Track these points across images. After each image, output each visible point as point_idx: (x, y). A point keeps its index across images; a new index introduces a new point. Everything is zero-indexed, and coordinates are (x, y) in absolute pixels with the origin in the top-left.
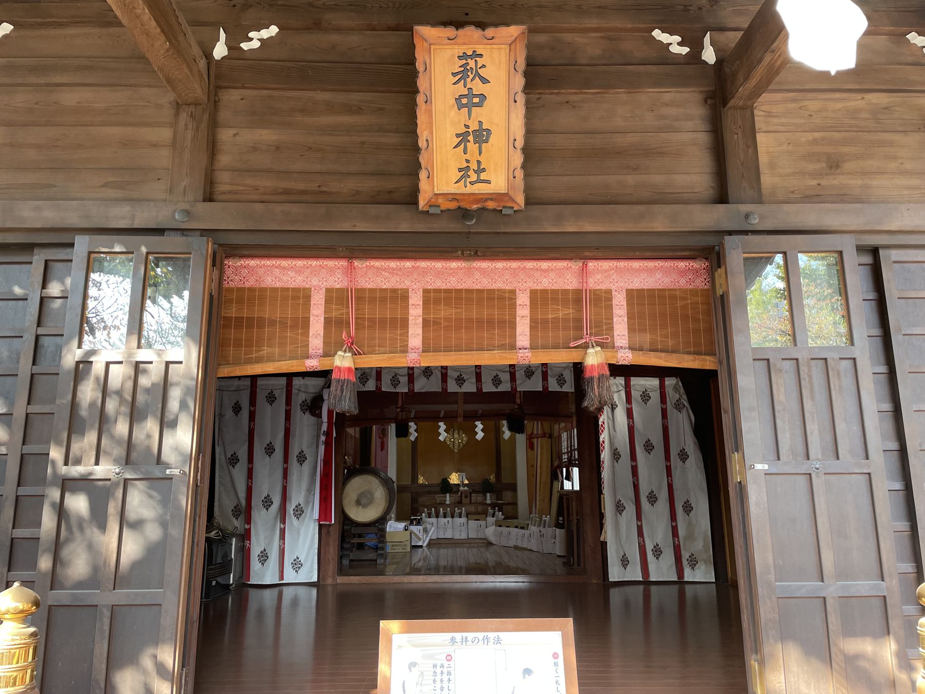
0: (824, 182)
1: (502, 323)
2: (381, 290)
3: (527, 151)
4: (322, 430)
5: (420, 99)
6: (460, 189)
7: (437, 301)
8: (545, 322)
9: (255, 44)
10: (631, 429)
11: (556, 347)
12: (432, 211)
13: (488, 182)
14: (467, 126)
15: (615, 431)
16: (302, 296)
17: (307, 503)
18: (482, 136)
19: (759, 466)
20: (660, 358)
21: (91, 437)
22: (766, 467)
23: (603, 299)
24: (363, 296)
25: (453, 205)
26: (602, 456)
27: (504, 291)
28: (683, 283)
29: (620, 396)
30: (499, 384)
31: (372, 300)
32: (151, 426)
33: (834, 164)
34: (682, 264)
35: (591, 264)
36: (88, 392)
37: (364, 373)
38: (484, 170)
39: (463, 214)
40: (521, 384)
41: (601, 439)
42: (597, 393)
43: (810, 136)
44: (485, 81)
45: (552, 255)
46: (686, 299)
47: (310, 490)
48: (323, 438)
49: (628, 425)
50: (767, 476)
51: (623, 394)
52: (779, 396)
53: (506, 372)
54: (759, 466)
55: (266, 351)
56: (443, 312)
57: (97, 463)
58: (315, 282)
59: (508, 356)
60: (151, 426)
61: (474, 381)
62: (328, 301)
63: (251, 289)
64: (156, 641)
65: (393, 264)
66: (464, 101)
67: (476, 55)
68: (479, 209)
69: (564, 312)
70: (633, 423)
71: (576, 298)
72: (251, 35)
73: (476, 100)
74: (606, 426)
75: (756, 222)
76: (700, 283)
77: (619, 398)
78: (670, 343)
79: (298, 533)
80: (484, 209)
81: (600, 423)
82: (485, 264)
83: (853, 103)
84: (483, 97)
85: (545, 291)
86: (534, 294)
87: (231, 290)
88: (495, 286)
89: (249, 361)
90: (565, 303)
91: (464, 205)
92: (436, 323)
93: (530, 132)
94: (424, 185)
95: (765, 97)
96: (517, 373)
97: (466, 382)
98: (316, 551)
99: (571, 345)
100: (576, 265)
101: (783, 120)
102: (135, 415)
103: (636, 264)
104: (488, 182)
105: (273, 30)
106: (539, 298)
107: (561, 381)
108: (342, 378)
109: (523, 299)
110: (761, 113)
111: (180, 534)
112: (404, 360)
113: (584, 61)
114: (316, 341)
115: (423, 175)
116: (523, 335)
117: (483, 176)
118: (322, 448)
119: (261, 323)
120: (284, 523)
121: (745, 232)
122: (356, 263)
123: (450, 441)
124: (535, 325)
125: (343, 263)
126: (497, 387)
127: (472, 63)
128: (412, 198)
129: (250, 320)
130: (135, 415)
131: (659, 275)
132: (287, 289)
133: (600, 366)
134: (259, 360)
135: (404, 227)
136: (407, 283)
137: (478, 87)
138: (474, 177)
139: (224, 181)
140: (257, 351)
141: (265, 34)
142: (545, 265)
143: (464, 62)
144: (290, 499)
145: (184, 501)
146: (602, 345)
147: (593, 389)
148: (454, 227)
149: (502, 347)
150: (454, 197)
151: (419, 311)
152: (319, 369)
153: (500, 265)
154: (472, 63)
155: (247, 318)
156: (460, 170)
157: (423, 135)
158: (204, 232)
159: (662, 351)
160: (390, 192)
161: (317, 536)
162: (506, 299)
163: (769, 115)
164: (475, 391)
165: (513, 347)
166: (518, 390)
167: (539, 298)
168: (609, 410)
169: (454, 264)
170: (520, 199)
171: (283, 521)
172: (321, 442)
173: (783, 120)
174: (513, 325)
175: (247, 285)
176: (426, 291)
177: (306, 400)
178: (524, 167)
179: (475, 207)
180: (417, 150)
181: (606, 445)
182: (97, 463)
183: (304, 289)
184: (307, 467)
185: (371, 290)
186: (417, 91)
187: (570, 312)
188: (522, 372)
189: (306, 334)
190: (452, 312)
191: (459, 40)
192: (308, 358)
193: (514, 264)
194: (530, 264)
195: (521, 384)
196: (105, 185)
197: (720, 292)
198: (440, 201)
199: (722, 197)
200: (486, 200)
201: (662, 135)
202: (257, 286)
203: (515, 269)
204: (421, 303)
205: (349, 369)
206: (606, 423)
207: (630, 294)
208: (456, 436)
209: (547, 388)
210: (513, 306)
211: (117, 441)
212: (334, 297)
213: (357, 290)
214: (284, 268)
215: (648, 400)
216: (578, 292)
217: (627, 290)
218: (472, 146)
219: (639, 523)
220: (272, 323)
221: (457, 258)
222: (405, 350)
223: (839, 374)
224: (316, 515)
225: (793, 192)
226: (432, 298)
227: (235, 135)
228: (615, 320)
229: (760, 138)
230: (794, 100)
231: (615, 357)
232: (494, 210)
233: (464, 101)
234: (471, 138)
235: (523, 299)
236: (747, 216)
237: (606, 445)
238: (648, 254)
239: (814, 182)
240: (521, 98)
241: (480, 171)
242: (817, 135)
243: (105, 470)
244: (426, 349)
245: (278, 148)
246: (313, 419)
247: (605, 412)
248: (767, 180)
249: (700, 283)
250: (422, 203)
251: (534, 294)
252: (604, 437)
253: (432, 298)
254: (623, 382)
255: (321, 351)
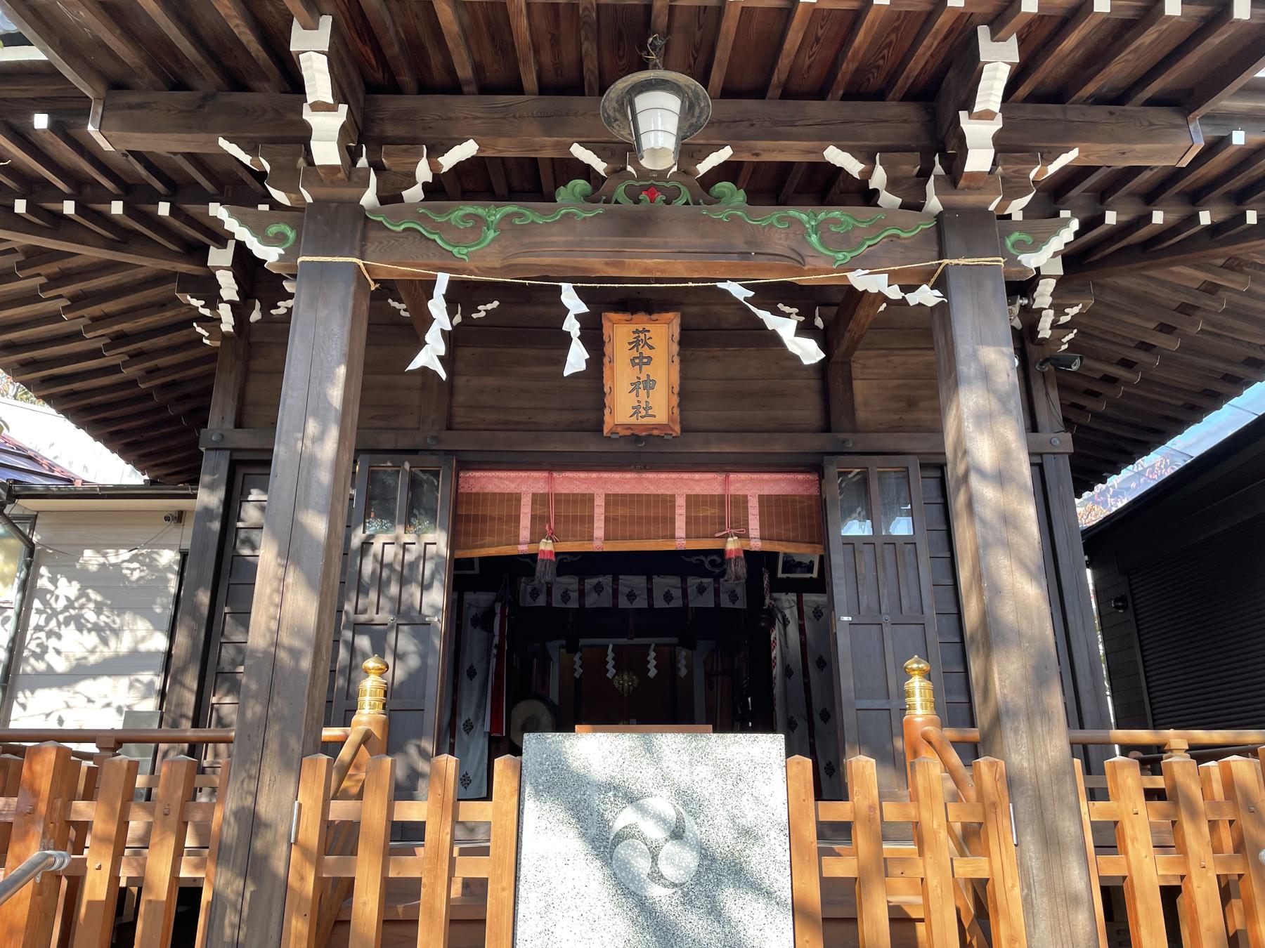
0: (903, 417)
1: (665, 520)
2: (573, 494)
3: (681, 394)
4: (494, 643)
5: (606, 360)
6: (633, 420)
7: (616, 503)
8: (697, 518)
9: (482, 314)
10: (803, 644)
11: (705, 537)
12: (613, 436)
13: (654, 416)
14: (638, 378)
15: (787, 647)
16: (515, 499)
17: (477, 718)
18: (649, 384)
19: (845, 619)
20: (782, 546)
21: (373, 595)
22: (850, 619)
23: (740, 502)
24: (560, 499)
25: (628, 433)
26: (774, 672)
27: (666, 495)
28: (800, 490)
29: (792, 612)
30: (671, 600)
31: (567, 502)
32: (415, 590)
33: (912, 404)
34: (801, 476)
35: (732, 476)
36: (368, 567)
37: (535, 588)
38: (651, 408)
39: (636, 439)
40: (694, 599)
41: (773, 655)
42: (733, 570)
43: (895, 383)
44: (651, 348)
45: (702, 469)
46: (804, 502)
47: (481, 705)
48: (495, 651)
49: (801, 641)
50: (851, 626)
51: (795, 609)
52: (861, 569)
53: (678, 588)
54: (845, 619)
55: (488, 539)
56: (620, 511)
57: (377, 613)
58: (524, 488)
59: (669, 543)
60: (415, 590)
61: (646, 596)
62: (534, 502)
63: (477, 494)
64: (419, 736)
65: (582, 475)
66: (637, 361)
67: (645, 331)
68: (647, 436)
69: (710, 512)
70: (805, 639)
71: (720, 501)
72: (480, 308)
73: (645, 360)
74: (778, 642)
75: (850, 446)
76: (814, 491)
77: (791, 613)
78: (791, 535)
79: (468, 749)
80: (650, 435)
81: (772, 639)
82: (651, 475)
83: (926, 358)
84: (650, 358)
85: (697, 496)
86: (688, 497)
87: (462, 494)
88: (659, 492)
89: (476, 547)
90: (712, 505)
91: (636, 432)
92: (615, 519)
93: (684, 378)
94: (607, 418)
95: (857, 353)
96: (689, 589)
97: (638, 598)
98: (486, 766)
99: (716, 535)
100: (720, 477)
101: (875, 371)
102: (403, 582)
103: (766, 476)
104: (654, 416)
105: (496, 304)
106: (693, 501)
107: (733, 597)
108: (546, 558)
109: (681, 502)
110: (858, 365)
111: (436, 663)
112: (591, 546)
113: (726, 326)
114: (525, 533)
115: (607, 411)
116: (680, 530)
117: (650, 412)
118: (493, 661)
119: (484, 519)
120: (454, 738)
121: (843, 454)
122: (555, 474)
123: (619, 683)
124: (689, 521)
125: (545, 474)
126: (668, 603)
127: (642, 336)
128: (598, 427)
129: (476, 517)
130: (403, 582)
131: (783, 485)
132: (504, 494)
133: (737, 550)
134: (483, 546)
135: (593, 448)
136: (592, 490)
137: (646, 352)
138: (644, 413)
139: (460, 416)
140: (481, 540)
141: (489, 307)
142: (697, 476)
143: (637, 335)
144: (460, 715)
145: (438, 643)
146: (739, 536)
147: (731, 567)
148: (630, 448)
149: (664, 537)
150: (629, 427)
151: (602, 510)
152: (528, 552)
153: (663, 476)
154: (642, 336)
155: (482, 515)
156: (633, 408)
157: (607, 384)
158: (448, 452)
159: (785, 541)
160: (581, 422)
161: (486, 751)
162: (669, 501)
163: (864, 367)
164: (646, 607)
165: (673, 537)
166: (690, 606)
167: (693, 501)
168: (781, 626)
169: (628, 475)
170: (678, 428)
171: (453, 736)
172: (492, 656)
173: (875, 371)
174: (673, 521)
175: (474, 491)
176: (607, 495)
177: (477, 615)
178: (680, 405)
179: (644, 434)
180: (604, 394)
181: (778, 661)
182: (377, 613)
183: (516, 494)
184: (477, 682)
185: (566, 495)
186: (604, 355)
187: (716, 511)
188: (694, 588)
189: (517, 527)
190: (627, 512)
191: (632, 322)
192: (519, 544)
193: (674, 476)
194: (686, 476)
195: (694, 599)
196: (372, 418)
197: (824, 497)
198: (619, 429)
199: (827, 428)
200: (652, 429)
201: (785, 381)
202: (481, 491)
203: (674, 479)
204: (603, 504)
205: (551, 552)
206: (778, 639)
207: (761, 498)
208: (626, 677)
209: (719, 604)
210: (673, 507)
211: (391, 599)
212: (538, 499)
213: (556, 494)
214: (501, 478)
215: (820, 616)
216: (722, 496)
217: (759, 495)
218: (642, 392)
219: (812, 741)
220: (492, 519)
221: (631, 471)
222: (591, 539)
223: (903, 554)
224: (487, 728)
225: (881, 424)
226: (611, 500)
227: (468, 381)
228: (750, 517)
229: (857, 384)
230: (884, 356)
231: (749, 544)
232: (658, 436)
233: (637, 361)
234: (641, 386)
235: (681, 502)
236: (844, 442)
237: (778, 661)
238: (788, 469)
239: (897, 417)
240: (677, 360)
241: (648, 408)
242: (900, 382)
243: (384, 617)
244: (607, 538)
245: (499, 390)
246: (484, 634)
247: (777, 628)
248: (862, 415)
249: (814, 491)
250: (606, 431)
251: (688, 497)
252: (776, 653)
253: (611, 500)
254: (795, 598)
255: (529, 540)
